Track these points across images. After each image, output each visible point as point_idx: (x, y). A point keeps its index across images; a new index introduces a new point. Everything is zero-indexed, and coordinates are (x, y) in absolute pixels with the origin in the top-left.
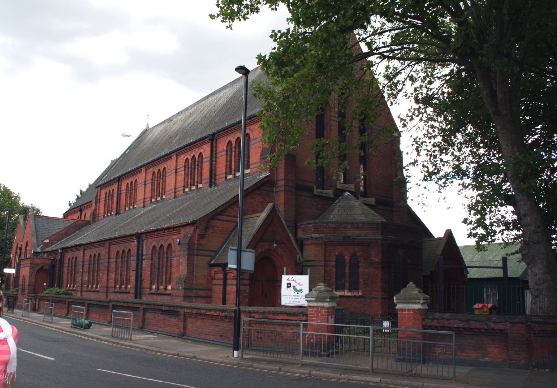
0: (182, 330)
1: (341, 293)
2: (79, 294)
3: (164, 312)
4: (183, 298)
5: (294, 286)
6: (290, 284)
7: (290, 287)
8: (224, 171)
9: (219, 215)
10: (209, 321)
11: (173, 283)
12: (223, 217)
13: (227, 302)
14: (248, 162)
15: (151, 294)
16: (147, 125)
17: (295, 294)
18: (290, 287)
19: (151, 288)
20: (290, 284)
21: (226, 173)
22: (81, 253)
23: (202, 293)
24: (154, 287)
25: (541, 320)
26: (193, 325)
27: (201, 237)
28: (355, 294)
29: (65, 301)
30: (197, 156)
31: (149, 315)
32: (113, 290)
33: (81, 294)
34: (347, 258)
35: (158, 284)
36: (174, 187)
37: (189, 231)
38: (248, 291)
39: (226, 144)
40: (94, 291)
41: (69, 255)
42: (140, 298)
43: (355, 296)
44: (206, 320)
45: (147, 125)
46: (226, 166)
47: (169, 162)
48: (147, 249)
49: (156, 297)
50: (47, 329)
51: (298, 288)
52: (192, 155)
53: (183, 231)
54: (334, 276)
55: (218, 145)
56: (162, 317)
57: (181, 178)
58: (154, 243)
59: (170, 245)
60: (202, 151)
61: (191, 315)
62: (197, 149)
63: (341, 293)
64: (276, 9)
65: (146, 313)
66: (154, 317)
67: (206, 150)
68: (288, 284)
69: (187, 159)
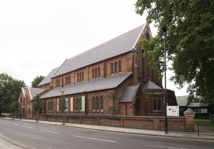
0: (122, 125)
1: (156, 111)
2: (56, 113)
3: (110, 119)
4: (112, 114)
5: (172, 110)
6: (170, 109)
7: (171, 110)
8: (110, 73)
9: (120, 86)
10: (136, 122)
11: (104, 109)
12: (121, 87)
13: (127, 115)
14: (83, 79)
15: (48, 112)
16: (66, 58)
17: (173, 112)
18: (171, 110)
19: (48, 111)
20: (170, 109)
21: (111, 73)
22: (55, 99)
23: (117, 112)
24: (51, 111)
25: (155, 93)
26: (126, 123)
27: (117, 93)
28: (160, 111)
29: (24, 115)
30: (69, 76)
31: (101, 120)
32: (47, 112)
33: (56, 114)
34: (157, 101)
35: (96, 109)
36: (88, 78)
37: (112, 92)
38: (135, 111)
39: (110, 64)
40: (51, 112)
41: (48, 101)
42: (88, 114)
43: (160, 112)
44: (134, 121)
45: (66, 58)
46: (111, 71)
47: (61, 77)
48: (47, 102)
49: (96, 114)
50: (99, 132)
51: (174, 110)
52: (95, 68)
53: (108, 92)
54: (153, 106)
55: (107, 64)
56: (109, 120)
57: (76, 79)
58: (93, 96)
59: (52, 101)
60: (100, 66)
61: (126, 120)
62: (97, 66)
63: (156, 111)
64: (135, 11)
65: (114, 119)
66: (105, 121)
67: (102, 66)
68: (169, 109)
69: (66, 77)
